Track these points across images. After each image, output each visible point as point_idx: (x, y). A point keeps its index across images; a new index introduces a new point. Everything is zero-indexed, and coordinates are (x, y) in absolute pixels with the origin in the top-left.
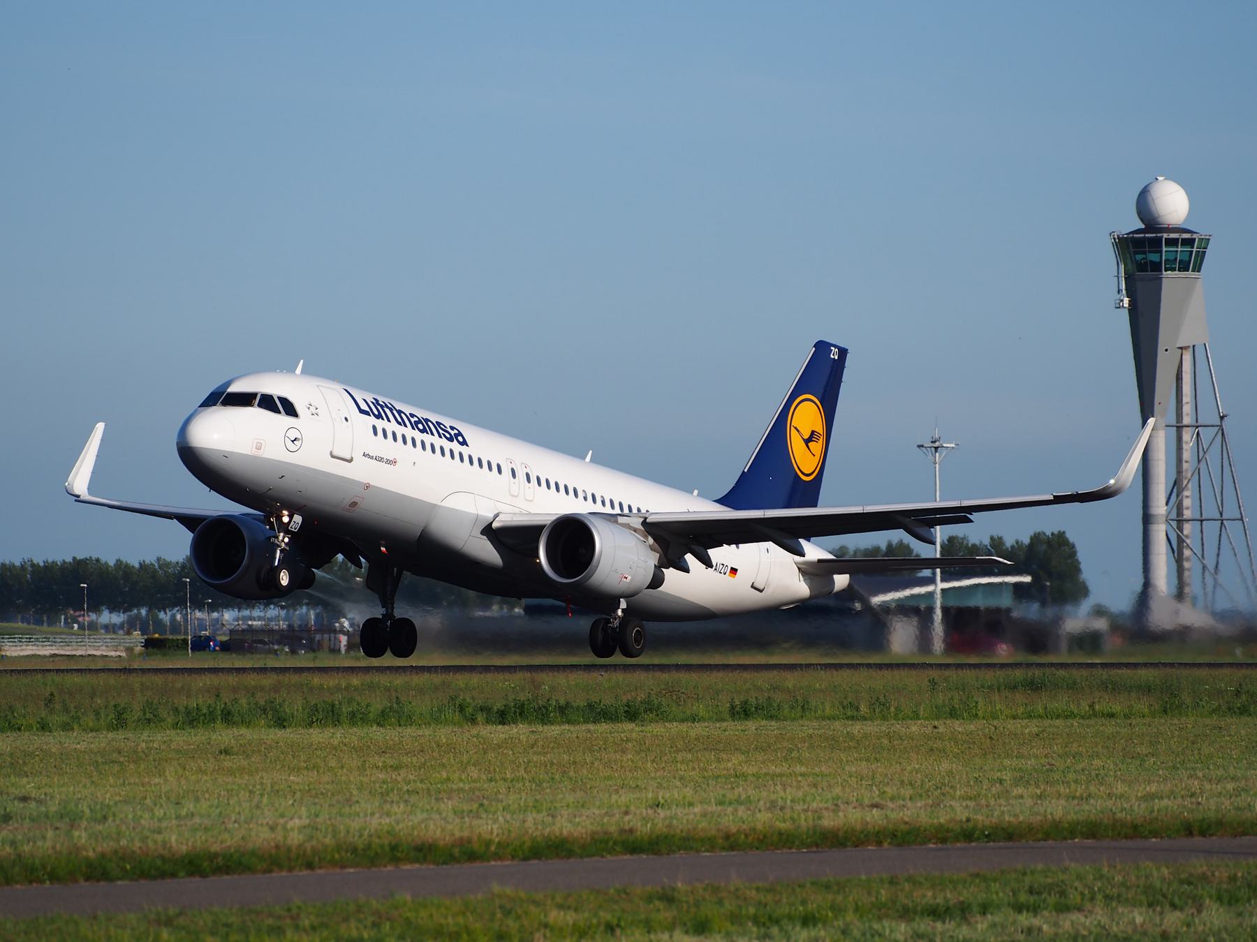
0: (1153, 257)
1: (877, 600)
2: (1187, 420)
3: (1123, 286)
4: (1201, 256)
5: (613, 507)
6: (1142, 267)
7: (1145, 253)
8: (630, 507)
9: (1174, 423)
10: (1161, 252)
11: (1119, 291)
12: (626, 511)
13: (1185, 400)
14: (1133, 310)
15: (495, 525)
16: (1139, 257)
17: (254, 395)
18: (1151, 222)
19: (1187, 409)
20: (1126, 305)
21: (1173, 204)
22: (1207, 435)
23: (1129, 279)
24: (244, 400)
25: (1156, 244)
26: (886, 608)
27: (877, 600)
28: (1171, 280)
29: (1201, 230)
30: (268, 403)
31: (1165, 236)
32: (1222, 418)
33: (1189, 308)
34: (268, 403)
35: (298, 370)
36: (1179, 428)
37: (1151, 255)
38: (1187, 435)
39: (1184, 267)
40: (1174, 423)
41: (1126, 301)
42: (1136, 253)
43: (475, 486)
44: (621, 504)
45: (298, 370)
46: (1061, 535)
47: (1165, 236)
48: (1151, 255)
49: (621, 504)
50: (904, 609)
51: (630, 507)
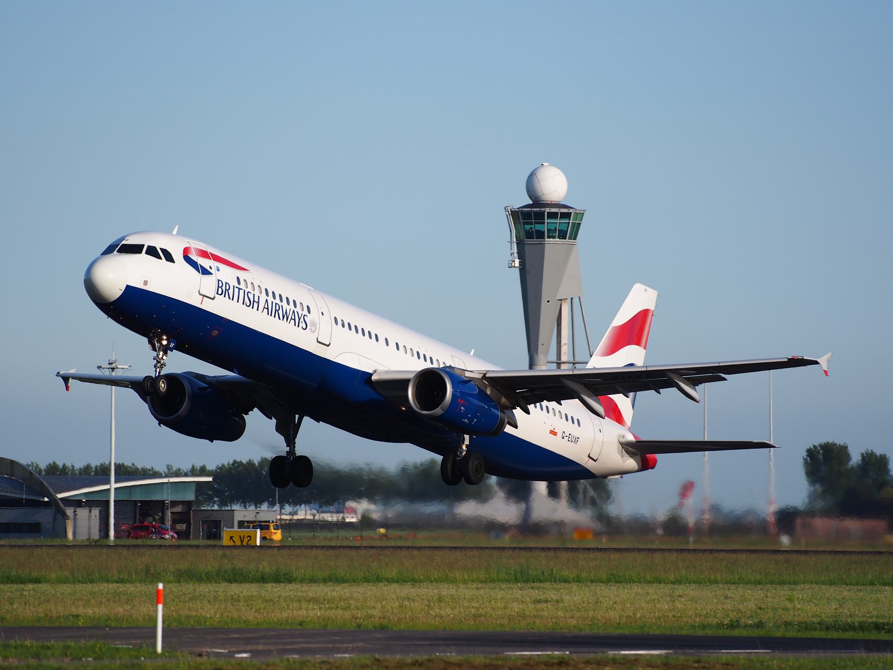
0: (538, 227)
1: (60, 496)
2: (564, 358)
3: (516, 251)
5: (432, 363)
6: (530, 235)
7: (531, 223)
10: (544, 223)
12: (238, 543)
14: (523, 269)
15: (374, 378)
16: (528, 227)
18: (537, 202)
19: (564, 349)
21: (555, 186)
23: (520, 244)
24: (136, 249)
25: (540, 217)
26: (76, 503)
27: (60, 496)
28: (552, 245)
29: (576, 204)
30: (152, 251)
31: (547, 210)
33: (573, 267)
34: (152, 251)
35: (175, 232)
37: (538, 225)
39: (563, 235)
40: (554, 359)
42: (525, 223)
44: (542, 409)
45: (175, 232)
47: (547, 210)
48: (538, 225)
49: (542, 409)
50: (91, 503)
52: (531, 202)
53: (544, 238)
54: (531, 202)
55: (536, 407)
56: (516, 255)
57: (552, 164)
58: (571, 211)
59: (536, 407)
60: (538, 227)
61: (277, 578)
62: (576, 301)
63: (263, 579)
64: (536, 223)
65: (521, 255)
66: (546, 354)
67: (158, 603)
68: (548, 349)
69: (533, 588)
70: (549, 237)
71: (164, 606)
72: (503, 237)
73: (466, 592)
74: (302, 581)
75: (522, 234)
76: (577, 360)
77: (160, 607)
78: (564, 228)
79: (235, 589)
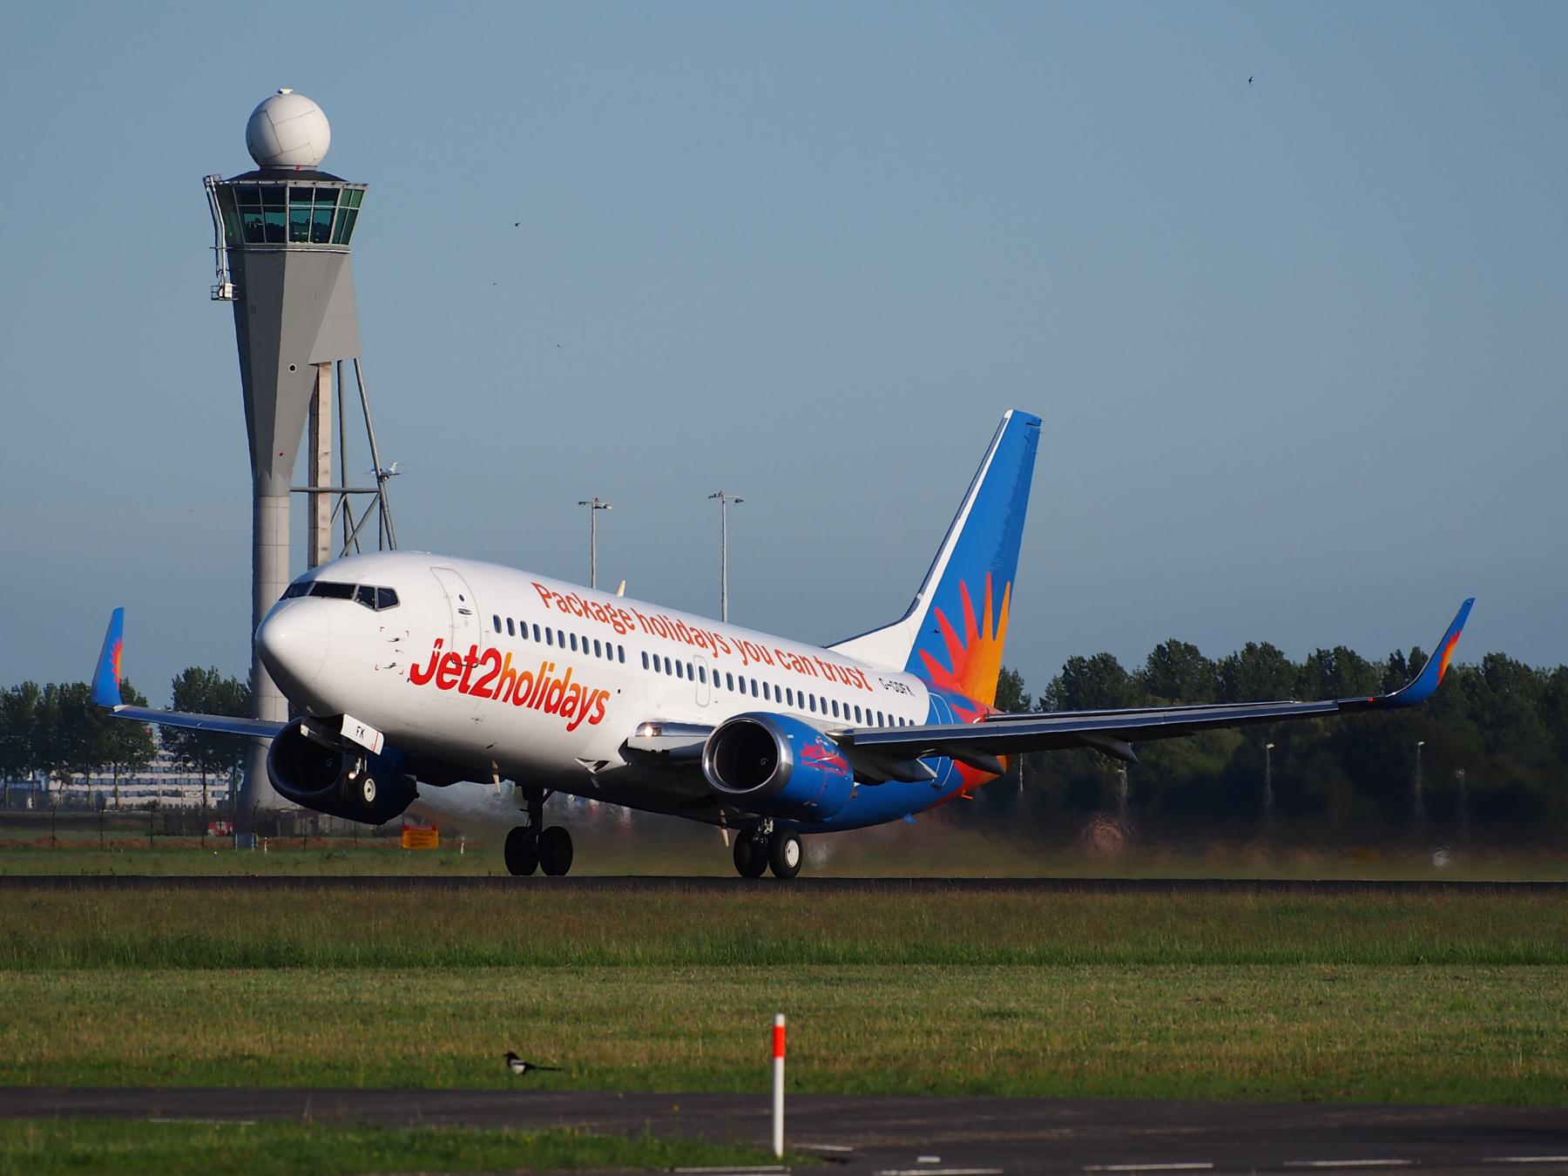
0: (272, 218)
2: (324, 482)
3: (226, 265)
4: (349, 219)
5: (859, 719)
6: (254, 234)
8: (901, 720)
9: (305, 484)
10: (284, 210)
11: (219, 272)
13: (322, 448)
16: (249, 218)
17: (353, 587)
18: (269, 164)
19: (324, 463)
20: (229, 295)
21: (305, 133)
22: (358, 504)
23: (234, 252)
24: (341, 591)
25: (275, 197)
28: (300, 257)
29: (350, 174)
31: (291, 184)
32: (380, 479)
33: (341, 303)
36: (314, 494)
37: (270, 214)
38: (325, 506)
39: (321, 235)
40: (305, 484)
41: (229, 288)
42: (244, 211)
43: (653, 688)
46: (189, 674)
47: (291, 184)
48: (270, 214)
51: (901, 720)
52: (257, 168)
53: (284, 241)
54: (257, 168)
55: (911, 722)
56: (226, 274)
57: (297, 91)
58: (337, 186)
59: (911, 722)
60: (272, 218)
61: (274, 959)
62: (348, 369)
63: (246, 961)
64: (266, 210)
65: (237, 275)
66: (288, 473)
67: (775, 1054)
68: (291, 465)
69: (766, 981)
70: (293, 239)
71: (786, 1063)
72: (200, 238)
73: (671, 991)
74: (324, 964)
75: (239, 232)
76: (349, 486)
77: (780, 1063)
78: (325, 221)
79: (202, 980)
